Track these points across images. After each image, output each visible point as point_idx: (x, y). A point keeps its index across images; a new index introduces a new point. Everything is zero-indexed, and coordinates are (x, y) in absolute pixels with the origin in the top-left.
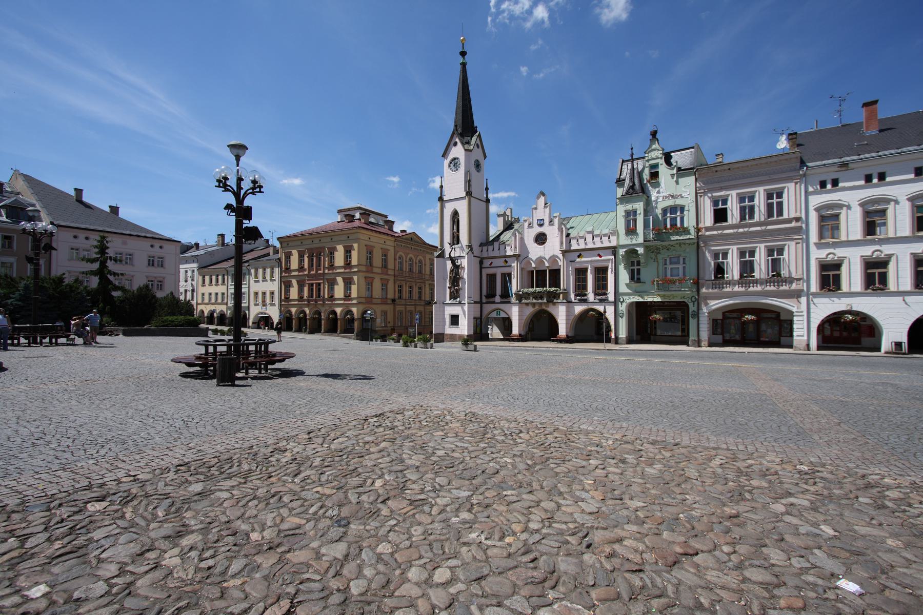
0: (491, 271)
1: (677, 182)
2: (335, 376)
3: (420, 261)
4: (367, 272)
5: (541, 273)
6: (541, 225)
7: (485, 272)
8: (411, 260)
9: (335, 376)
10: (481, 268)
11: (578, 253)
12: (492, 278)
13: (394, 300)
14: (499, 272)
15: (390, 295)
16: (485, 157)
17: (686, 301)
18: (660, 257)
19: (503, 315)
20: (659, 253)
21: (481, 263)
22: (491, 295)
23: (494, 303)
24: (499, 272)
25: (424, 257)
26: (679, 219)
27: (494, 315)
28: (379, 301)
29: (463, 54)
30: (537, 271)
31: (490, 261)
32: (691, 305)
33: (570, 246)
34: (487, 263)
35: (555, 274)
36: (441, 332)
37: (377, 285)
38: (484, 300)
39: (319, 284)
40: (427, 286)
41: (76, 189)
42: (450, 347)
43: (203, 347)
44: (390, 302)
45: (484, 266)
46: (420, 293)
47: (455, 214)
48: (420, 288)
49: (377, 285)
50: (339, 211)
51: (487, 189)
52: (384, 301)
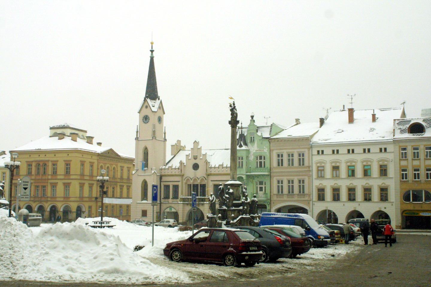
1: (262, 143)
3: (114, 168)
4: (81, 179)
5: (195, 187)
8: (108, 167)
10: (161, 182)
13: (96, 198)
15: (94, 195)
16: (164, 113)
17: (265, 204)
18: (254, 181)
19: (173, 210)
20: (254, 179)
25: (117, 165)
27: (168, 210)
28: (87, 199)
29: (152, 51)
30: (200, 185)
32: (267, 206)
34: (164, 179)
35: (203, 187)
37: (86, 188)
39: (44, 187)
40: (118, 186)
41: (76, 141)
42: (110, 213)
44: (94, 199)
45: (162, 180)
46: (113, 192)
47: (146, 149)
48: (113, 188)
49: (86, 188)
50: (185, 146)
51: (165, 133)
52: (90, 198)
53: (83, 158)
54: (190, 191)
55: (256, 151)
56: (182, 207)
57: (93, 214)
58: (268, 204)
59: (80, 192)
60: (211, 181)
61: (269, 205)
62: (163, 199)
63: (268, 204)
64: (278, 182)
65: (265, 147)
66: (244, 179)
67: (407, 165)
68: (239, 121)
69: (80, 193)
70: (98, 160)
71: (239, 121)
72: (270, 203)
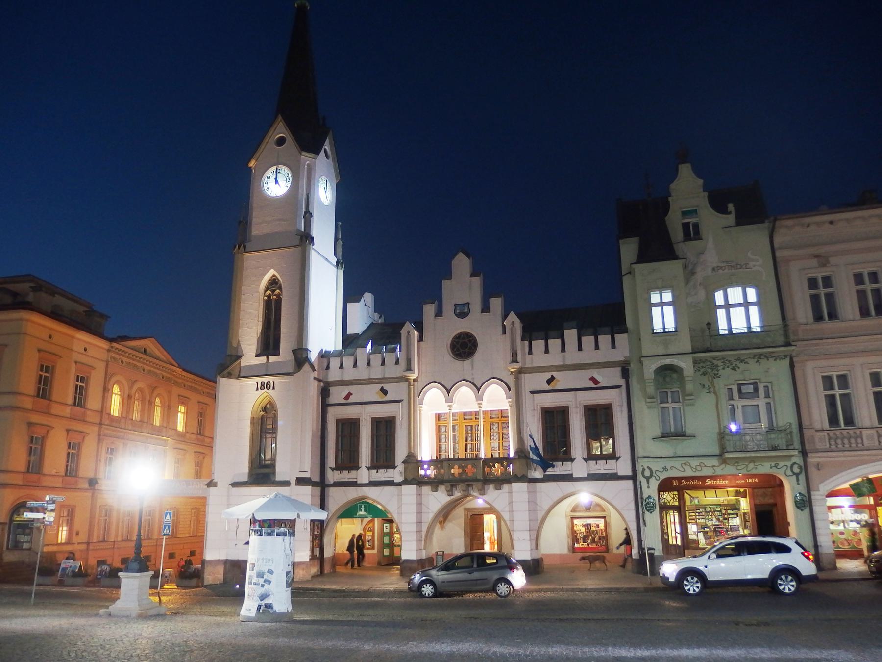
0: (350, 412)
2: (327, 259)
6: (462, 315)
7: (334, 414)
9: (327, 259)
11: (548, 375)
12: (349, 429)
14: (366, 415)
20: (717, 376)
21: (325, 393)
22: (348, 461)
23: (354, 484)
24: (366, 415)
26: (331, 461)
31: (345, 391)
33: (525, 364)
34: (337, 394)
36: (241, 557)
38: (332, 476)
43: (630, 473)
45: (332, 399)
53: (52, 343)
54: (842, 335)
55: (713, 269)
56: (525, 496)
57: (77, 534)
58: (794, 473)
59: (67, 462)
60: (532, 392)
61: (797, 475)
62: (333, 469)
63: (794, 473)
64: (828, 382)
65: (749, 254)
66: (685, 373)
67: (279, 477)
68: (473, 275)
69: (67, 466)
70: (107, 362)
71: (473, 275)
72: (800, 467)
